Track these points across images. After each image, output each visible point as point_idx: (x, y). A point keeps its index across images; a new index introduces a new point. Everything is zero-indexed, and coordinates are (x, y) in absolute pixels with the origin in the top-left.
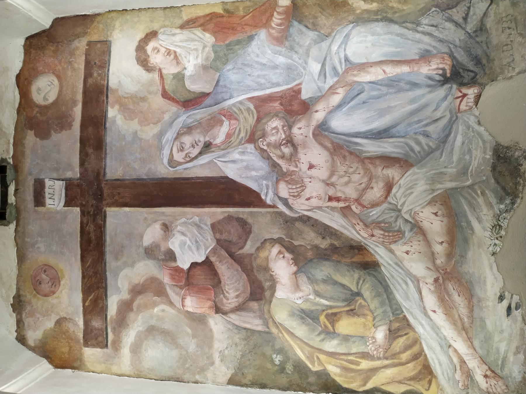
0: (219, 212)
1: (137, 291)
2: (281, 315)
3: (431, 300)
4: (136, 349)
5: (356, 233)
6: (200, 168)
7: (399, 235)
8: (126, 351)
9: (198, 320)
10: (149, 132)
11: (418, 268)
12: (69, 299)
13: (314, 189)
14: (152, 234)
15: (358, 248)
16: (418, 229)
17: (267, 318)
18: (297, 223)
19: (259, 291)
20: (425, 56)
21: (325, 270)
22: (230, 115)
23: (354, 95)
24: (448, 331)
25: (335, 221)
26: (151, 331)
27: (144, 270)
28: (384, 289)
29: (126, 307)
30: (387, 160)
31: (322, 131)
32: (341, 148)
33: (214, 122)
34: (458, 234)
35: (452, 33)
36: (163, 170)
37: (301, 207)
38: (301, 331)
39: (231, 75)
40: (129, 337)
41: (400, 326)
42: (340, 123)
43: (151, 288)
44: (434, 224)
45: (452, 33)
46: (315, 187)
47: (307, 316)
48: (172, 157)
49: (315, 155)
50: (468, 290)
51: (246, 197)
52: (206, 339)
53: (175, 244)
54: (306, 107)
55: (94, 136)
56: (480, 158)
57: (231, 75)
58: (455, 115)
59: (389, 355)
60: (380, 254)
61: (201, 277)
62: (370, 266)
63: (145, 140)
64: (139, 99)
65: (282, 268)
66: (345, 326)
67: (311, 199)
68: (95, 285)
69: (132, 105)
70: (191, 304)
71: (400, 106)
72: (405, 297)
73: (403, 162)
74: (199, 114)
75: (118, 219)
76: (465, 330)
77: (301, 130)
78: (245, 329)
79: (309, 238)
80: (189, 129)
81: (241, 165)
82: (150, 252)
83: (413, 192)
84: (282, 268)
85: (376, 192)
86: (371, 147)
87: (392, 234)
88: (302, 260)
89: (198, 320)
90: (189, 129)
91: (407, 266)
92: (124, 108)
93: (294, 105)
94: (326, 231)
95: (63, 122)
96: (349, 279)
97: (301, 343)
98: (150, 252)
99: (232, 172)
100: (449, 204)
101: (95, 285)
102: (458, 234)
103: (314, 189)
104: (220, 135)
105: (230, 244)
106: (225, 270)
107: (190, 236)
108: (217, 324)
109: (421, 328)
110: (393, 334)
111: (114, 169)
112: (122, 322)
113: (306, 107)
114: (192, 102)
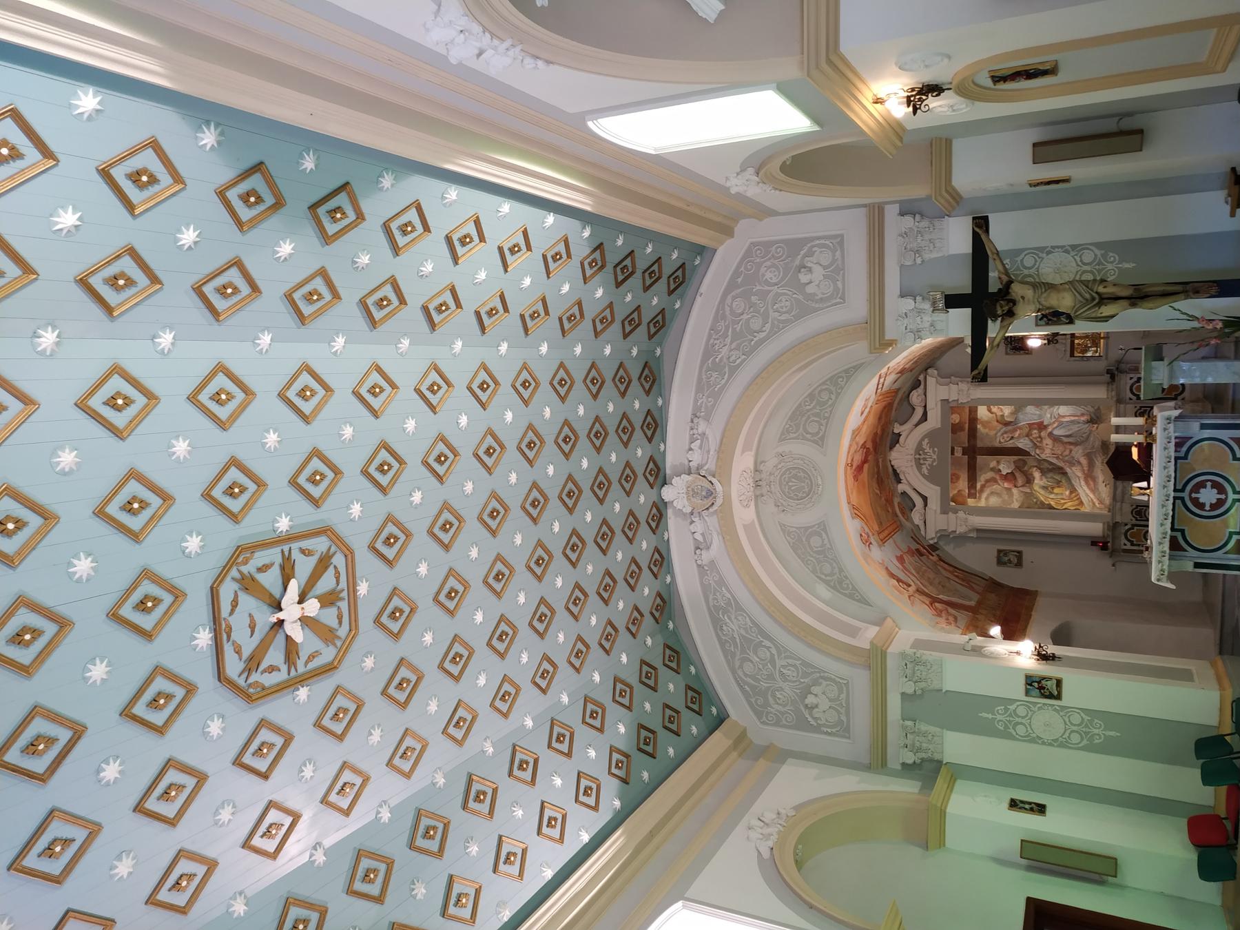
0: (1016, 458)
1: (987, 481)
2: (1036, 488)
3: (1083, 483)
4: (987, 499)
5: (1061, 464)
6: (1010, 444)
7: (1074, 465)
8: (983, 499)
9: (1009, 490)
10: (992, 433)
11: (1080, 474)
12: (963, 484)
13: (1048, 451)
14: (993, 464)
15: (1061, 468)
16: (1079, 462)
17: (1031, 489)
18: (1154, 377)
19: (1029, 481)
20: (1083, 415)
21: (1050, 475)
22: (1020, 428)
23: (1061, 424)
24: (1088, 491)
25: (1054, 461)
26: (992, 493)
27: (990, 475)
28: (1069, 480)
29: (983, 487)
30: (1070, 443)
31: (1050, 434)
32: (1056, 439)
33: (1015, 430)
34: (1091, 465)
35: (1092, 410)
36: (997, 445)
37: (1043, 456)
38: (1042, 492)
39: (1021, 416)
40: (984, 495)
41: (1073, 490)
42: (1056, 432)
43: (994, 480)
44: (1084, 461)
45: (1092, 410)
46: (1048, 451)
47: (1044, 488)
48: (1000, 439)
49: (1048, 441)
50: (1094, 479)
51: (1026, 453)
52: (1011, 495)
53: (1001, 467)
54: (1046, 427)
55: (973, 432)
56: (1098, 444)
57: (1021, 416)
58: (1091, 432)
59: (1071, 499)
60: (1068, 470)
61: (1010, 477)
62: (1065, 474)
63: (990, 434)
64: (988, 422)
65: (1037, 474)
66: (1056, 491)
67: (1046, 454)
68: (972, 480)
69: (986, 424)
70: (1006, 485)
71: (1075, 428)
72: (1075, 482)
73: (1075, 444)
74: (1010, 428)
75: (980, 459)
76: (1093, 491)
77: (1043, 434)
78: (817, 729)
79: (1046, 465)
80: (1006, 432)
81: (1023, 444)
82: (992, 469)
83: (1078, 453)
84: (1037, 474)
85: (1067, 452)
86: (1065, 440)
87: (1071, 464)
88: (1044, 472)
89: (1009, 490)
90: (1006, 432)
91: (1076, 473)
92: (984, 427)
93: (1041, 426)
94: (1051, 463)
95: (962, 429)
96: (1058, 477)
97: (1042, 495)
98: (992, 469)
99: (1020, 446)
100: (1089, 457)
101: (972, 480)
102: (1091, 465)
103: (1048, 451)
104: (1017, 434)
105: (1020, 467)
106: (1017, 475)
107: (1006, 466)
108: (1015, 491)
109: (1080, 491)
110: (1071, 492)
111: (980, 444)
112: (982, 491)
113: (1046, 427)
114: (1007, 424)
